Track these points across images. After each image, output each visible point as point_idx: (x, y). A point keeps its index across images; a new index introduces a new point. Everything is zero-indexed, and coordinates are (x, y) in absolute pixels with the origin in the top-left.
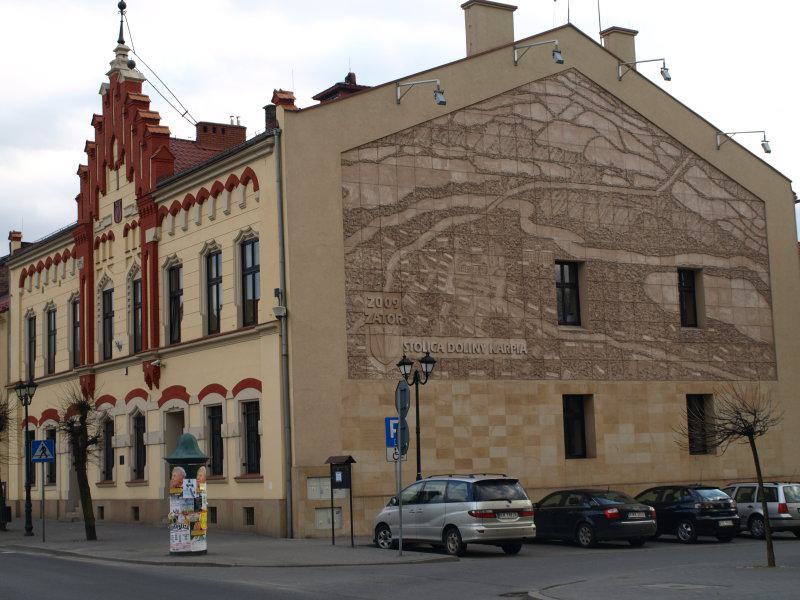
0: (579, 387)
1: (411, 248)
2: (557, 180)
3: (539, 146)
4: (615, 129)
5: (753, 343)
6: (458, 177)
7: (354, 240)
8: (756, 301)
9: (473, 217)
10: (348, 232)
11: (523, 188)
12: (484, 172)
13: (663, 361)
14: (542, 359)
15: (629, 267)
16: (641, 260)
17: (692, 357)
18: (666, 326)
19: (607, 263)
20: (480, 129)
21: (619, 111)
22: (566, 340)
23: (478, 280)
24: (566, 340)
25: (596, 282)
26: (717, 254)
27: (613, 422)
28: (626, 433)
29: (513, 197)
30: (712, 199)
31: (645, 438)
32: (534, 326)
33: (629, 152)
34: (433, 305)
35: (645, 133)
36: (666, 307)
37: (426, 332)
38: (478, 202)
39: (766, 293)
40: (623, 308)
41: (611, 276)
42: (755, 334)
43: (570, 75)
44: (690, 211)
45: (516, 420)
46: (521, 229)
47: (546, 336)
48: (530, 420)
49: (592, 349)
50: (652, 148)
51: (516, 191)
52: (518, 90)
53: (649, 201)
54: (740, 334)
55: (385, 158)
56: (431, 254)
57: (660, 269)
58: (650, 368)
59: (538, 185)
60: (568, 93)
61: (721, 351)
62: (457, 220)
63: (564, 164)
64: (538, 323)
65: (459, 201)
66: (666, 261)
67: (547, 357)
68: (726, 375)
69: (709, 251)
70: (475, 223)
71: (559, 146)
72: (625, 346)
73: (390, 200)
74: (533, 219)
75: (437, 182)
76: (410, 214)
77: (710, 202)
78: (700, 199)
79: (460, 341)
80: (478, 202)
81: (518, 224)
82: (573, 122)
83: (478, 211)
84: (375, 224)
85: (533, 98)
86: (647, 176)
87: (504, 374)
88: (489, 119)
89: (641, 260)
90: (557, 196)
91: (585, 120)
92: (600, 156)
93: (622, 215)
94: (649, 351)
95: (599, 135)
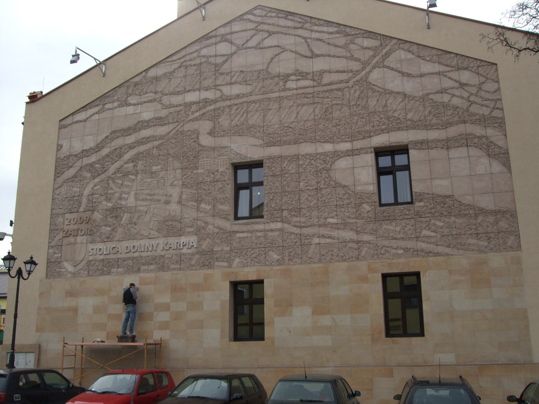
0: (249, 273)
1: (103, 176)
2: (238, 96)
3: (222, 74)
4: (303, 41)
5: (483, 211)
6: (146, 116)
7: (60, 180)
8: (484, 165)
9: (156, 143)
10: (58, 173)
11: (203, 111)
12: (171, 106)
13: (352, 241)
14: (212, 251)
15: (313, 157)
16: (328, 147)
17: (391, 234)
18: (358, 206)
19: (286, 157)
20: (169, 75)
21: (307, 25)
22: (238, 232)
23: (157, 191)
24: (238, 232)
25: (274, 176)
26: (428, 127)
27: (286, 306)
28: (301, 315)
29: (193, 120)
30: (422, 76)
31: (326, 320)
32: (206, 223)
33: (318, 56)
34: (116, 217)
35: (338, 35)
36: (359, 188)
37: (109, 239)
38: (162, 130)
39: (503, 157)
40: (304, 196)
41: (292, 168)
42: (486, 202)
43: (256, 12)
44: (391, 92)
45: (182, 306)
46: (199, 144)
47: (216, 230)
48: (195, 306)
49: (265, 237)
50: (345, 47)
51: (197, 114)
52: (206, 37)
53: (340, 94)
54: (461, 204)
55: (91, 116)
56: (119, 178)
57: (352, 153)
58: (335, 250)
59: (218, 105)
60: (253, 26)
61: (434, 224)
62: (142, 148)
63: (245, 82)
64: (210, 219)
65: (145, 133)
66: (358, 144)
67: (216, 249)
68: (440, 249)
69: (415, 126)
70: (157, 148)
71: (241, 69)
72: (305, 231)
73: (92, 144)
74: (211, 133)
75: (131, 123)
76: (105, 151)
77: (418, 80)
78: (405, 79)
79: (136, 243)
80: (162, 130)
81: (197, 140)
82: (258, 47)
83: (162, 137)
84: (79, 164)
85: (219, 39)
86: (337, 72)
87: (172, 266)
88: (176, 66)
89: (328, 147)
90: (236, 110)
91: (268, 42)
92: (286, 64)
93: (306, 112)
94: (335, 233)
95: (284, 50)
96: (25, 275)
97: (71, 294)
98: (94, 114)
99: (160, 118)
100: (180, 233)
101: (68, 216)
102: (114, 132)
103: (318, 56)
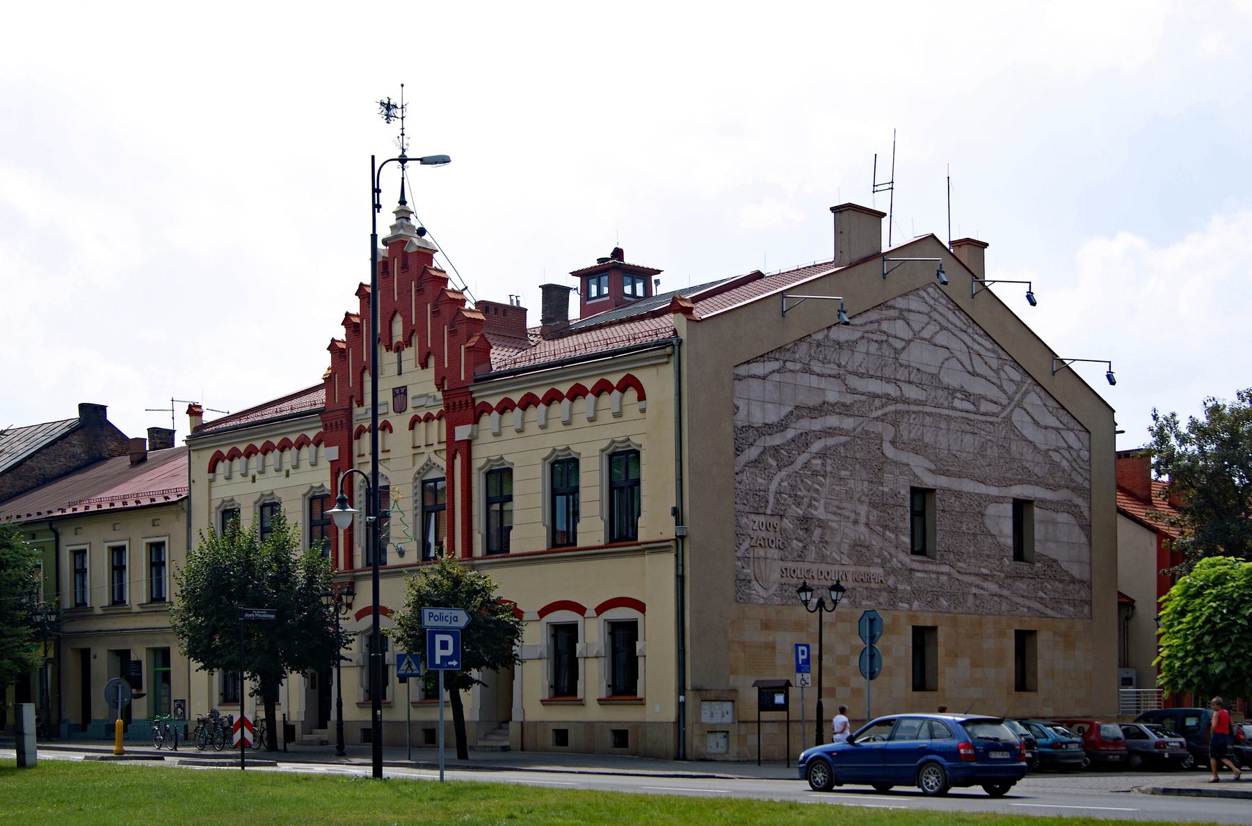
6: (832, 397)
12: (854, 392)
27: (954, 655)
56: (807, 476)
65: (832, 421)
75: (814, 401)
96: (829, 606)
97: (766, 626)
99: (844, 405)
101: (753, 517)
103: (978, 375)
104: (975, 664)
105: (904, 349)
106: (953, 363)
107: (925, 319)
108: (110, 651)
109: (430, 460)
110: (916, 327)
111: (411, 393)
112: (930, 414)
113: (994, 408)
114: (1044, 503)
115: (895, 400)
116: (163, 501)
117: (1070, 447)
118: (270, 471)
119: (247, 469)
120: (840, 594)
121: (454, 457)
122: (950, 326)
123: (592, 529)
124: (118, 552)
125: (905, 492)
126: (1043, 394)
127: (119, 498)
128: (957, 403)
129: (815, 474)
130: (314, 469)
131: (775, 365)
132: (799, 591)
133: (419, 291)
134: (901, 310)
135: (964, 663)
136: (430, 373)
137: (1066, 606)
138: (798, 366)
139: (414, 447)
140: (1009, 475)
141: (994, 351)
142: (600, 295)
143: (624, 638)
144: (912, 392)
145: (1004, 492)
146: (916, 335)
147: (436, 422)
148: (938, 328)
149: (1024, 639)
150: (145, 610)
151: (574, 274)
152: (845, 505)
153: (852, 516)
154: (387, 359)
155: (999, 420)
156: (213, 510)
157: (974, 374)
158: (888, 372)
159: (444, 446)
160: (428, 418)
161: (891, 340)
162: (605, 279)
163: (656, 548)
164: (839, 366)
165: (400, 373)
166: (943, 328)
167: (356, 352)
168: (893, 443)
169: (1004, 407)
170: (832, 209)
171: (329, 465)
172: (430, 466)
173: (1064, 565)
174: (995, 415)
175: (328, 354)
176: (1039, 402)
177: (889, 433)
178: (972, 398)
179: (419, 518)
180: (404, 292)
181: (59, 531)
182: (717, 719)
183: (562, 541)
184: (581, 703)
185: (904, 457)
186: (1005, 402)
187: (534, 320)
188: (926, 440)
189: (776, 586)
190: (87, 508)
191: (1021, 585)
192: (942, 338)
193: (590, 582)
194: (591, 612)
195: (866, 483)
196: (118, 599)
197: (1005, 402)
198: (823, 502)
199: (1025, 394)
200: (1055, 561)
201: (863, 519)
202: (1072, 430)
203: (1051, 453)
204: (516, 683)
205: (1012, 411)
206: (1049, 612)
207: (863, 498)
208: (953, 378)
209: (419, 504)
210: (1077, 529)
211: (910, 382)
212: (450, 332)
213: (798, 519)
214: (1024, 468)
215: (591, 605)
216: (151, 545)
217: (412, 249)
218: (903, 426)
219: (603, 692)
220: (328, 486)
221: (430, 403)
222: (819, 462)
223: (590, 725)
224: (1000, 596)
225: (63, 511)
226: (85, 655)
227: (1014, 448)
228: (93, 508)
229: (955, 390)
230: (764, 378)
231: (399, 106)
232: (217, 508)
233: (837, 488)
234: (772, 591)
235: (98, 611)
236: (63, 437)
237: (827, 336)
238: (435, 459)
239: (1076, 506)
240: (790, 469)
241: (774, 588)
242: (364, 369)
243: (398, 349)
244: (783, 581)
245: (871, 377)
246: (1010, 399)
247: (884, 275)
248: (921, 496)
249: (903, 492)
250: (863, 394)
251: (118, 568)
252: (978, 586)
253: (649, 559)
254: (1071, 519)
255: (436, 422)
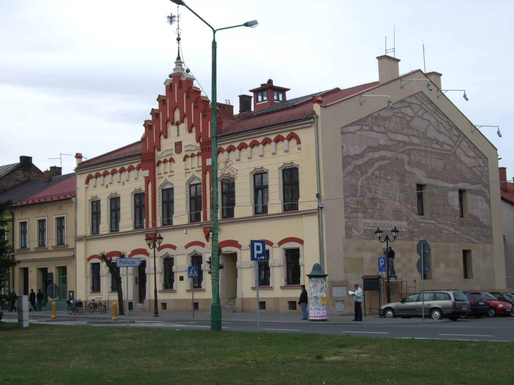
6: (382, 142)
10: (344, 167)
12: (391, 140)
49: (429, 226)
65: (383, 153)
75: (374, 144)
93: (440, 164)
97: (359, 250)
98: (356, 131)
99: (387, 146)
100: (401, 220)
101: (352, 198)
102: (368, 147)
104: (447, 266)
105: (411, 121)
106: (431, 127)
107: (418, 107)
108: (38, 269)
109: (193, 175)
110: (416, 111)
111: (183, 145)
112: (423, 151)
113: (449, 148)
114: (471, 191)
115: (409, 144)
116: (64, 198)
117: (480, 166)
118: (115, 183)
119: (104, 182)
120: (397, 233)
121: (206, 173)
122: (429, 111)
123: (104, 227)
124: (42, 222)
125: (414, 186)
126: (468, 141)
127: (42, 197)
128: (434, 146)
129: (377, 178)
130: (134, 181)
131: (358, 127)
132: (376, 233)
133: (187, 98)
134: (409, 103)
135: (442, 265)
136: (193, 135)
137: (482, 238)
138: (368, 128)
139: (186, 170)
140: (456, 178)
141: (447, 122)
142: (263, 100)
143: (293, 257)
144: (415, 140)
145: (454, 185)
146: (416, 115)
147: (196, 157)
148: (424, 111)
149: (466, 253)
150: (37, 251)
151: (251, 91)
152: (390, 192)
153: (393, 197)
154: (172, 129)
155: (451, 153)
156: (88, 201)
157: (440, 132)
158: (405, 131)
159: (201, 168)
160: (193, 156)
161: (406, 117)
162: (265, 93)
163: (308, 213)
164: (385, 128)
165: (178, 136)
166: (426, 111)
167: (156, 125)
168: (408, 163)
169: (453, 147)
170: (377, 58)
171: (144, 179)
172: (193, 178)
173: (481, 220)
174: (450, 151)
175: (144, 128)
176: (467, 145)
177: (406, 158)
178: (439, 143)
179: (188, 202)
180: (180, 98)
181: (14, 213)
182: (339, 295)
183: (261, 211)
184: (272, 288)
185: (413, 170)
186: (453, 145)
187: (236, 111)
188: (422, 162)
189: (362, 230)
190: (27, 202)
191: (464, 228)
192: (426, 116)
193: (275, 231)
194: (276, 244)
195: (398, 182)
196: (42, 244)
197: (453, 145)
198: (380, 190)
199: (461, 141)
200: (477, 217)
201: (398, 199)
202: (481, 158)
203: (473, 168)
204: (238, 280)
205: (456, 149)
206: (475, 241)
207: (397, 189)
208: (432, 134)
209: (188, 196)
210: (485, 203)
211: (414, 136)
212: (203, 116)
213: (370, 198)
214: (462, 175)
215: (275, 242)
216: (58, 219)
217: (184, 79)
218: (412, 156)
219: (283, 283)
220: (143, 188)
221: (193, 148)
222: (378, 172)
223: (276, 300)
224: (455, 234)
225: (16, 204)
226: (25, 271)
227: (458, 166)
228: (30, 202)
229: (432, 140)
230: (354, 133)
231: (177, 16)
232: (90, 201)
233: (387, 184)
234: (361, 233)
235: (32, 250)
236: (13, 171)
237: (379, 114)
238: (196, 174)
239: (484, 192)
240: (366, 176)
241: (362, 232)
242: (161, 134)
243: (178, 124)
244: (365, 228)
245: (398, 133)
246: (455, 143)
247: (402, 87)
248: (420, 187)
249: (413, 186)
250: (395, 141)
251: (42, 231)
252: (446, 230)
253: (305, 219)
254: (483, 199)
255: (196, 157)
